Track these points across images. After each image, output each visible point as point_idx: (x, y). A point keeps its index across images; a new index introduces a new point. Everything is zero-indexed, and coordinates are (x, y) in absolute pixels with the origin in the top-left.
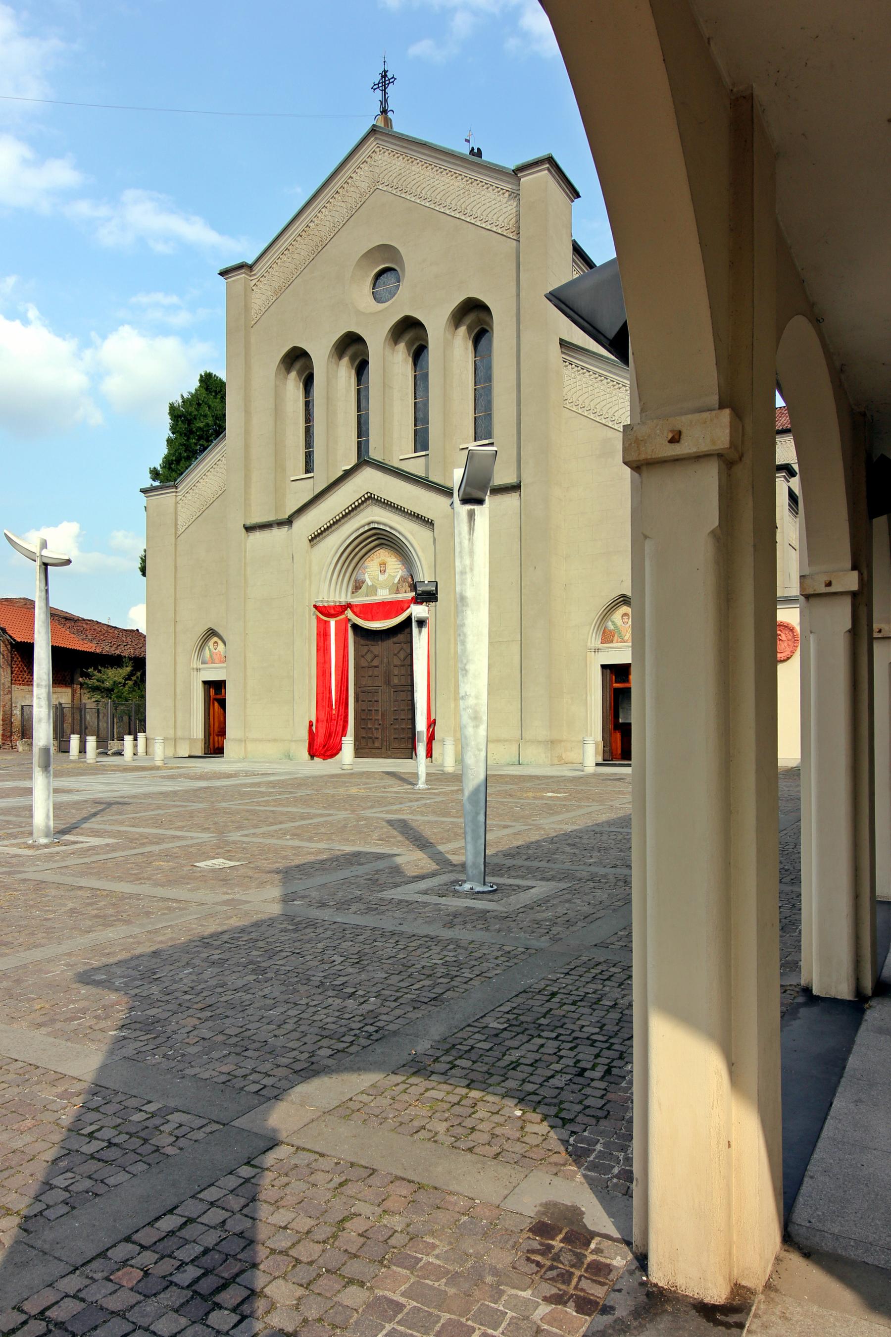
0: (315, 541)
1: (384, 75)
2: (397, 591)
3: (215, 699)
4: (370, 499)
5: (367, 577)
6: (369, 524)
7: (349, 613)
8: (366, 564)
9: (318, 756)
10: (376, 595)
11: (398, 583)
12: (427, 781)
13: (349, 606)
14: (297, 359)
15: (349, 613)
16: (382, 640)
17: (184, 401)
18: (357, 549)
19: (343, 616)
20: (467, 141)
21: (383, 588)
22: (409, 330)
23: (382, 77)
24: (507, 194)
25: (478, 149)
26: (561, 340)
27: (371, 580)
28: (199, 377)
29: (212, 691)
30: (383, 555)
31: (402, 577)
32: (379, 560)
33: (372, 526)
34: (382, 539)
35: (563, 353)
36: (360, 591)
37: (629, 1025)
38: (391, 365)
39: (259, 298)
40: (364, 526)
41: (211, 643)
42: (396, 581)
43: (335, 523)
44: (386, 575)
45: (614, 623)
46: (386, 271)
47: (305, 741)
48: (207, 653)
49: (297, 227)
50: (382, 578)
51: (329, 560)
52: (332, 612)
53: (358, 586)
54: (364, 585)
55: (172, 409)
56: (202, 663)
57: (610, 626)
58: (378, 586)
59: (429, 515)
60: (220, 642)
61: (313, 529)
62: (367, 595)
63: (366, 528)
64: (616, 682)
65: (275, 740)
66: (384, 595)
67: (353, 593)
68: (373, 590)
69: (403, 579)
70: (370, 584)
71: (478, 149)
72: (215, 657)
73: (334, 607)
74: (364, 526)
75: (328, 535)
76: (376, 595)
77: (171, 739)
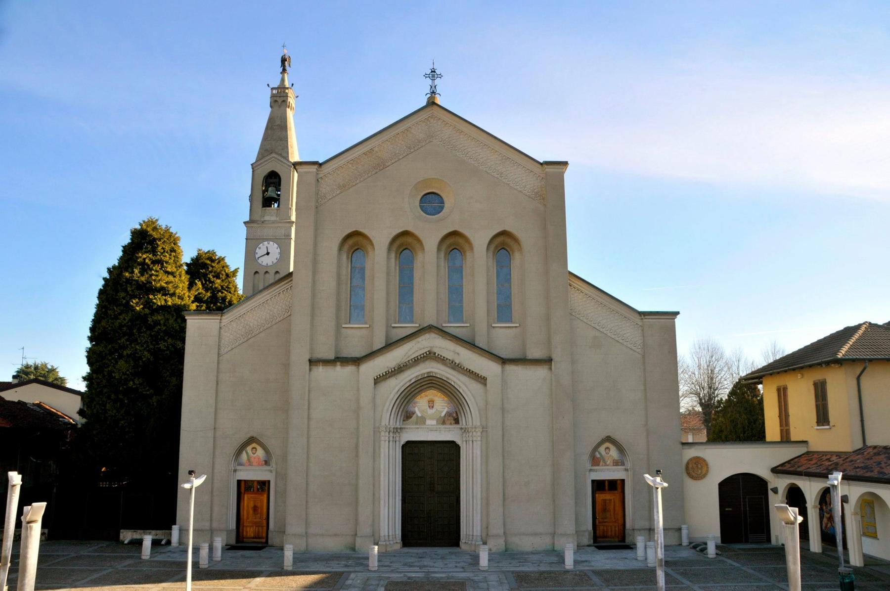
5: (416, 410)
8: (416, 400)
14: (355, 242)
17: (192, 259)
22: (454, 243)
27: (420, 412)
30: (432, 394)
31: (447, 412)
34: (430, 382)
37: (279, 552)
41: (249, 449)
42: (443, 414)
44: (434, 410)
45: (600, 453)
46: (431, 202)
48: (244, 456)
50: (430, 412)
51: (392, 396)
54: (414, 416)
55: (109, 269)
59: (482, 373)
60: (258, 448)
61: (381, 371)
65: (336, 535)
69: (449, 414)
70: (419, 415)
72: (252, 460)
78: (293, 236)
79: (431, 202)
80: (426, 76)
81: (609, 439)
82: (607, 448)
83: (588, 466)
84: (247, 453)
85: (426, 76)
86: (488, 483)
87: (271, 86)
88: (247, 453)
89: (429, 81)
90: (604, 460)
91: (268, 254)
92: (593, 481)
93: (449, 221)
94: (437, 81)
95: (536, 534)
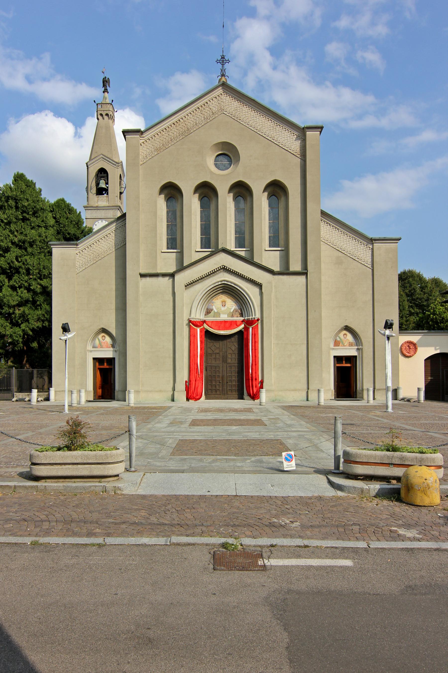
0: (188, 287)
1: (223, 57)
2: (232, 316)
3: (99, 369)
4: (225, 269)
5: (214, 307)
6: (221, 281)
7: (205, 326)
8: (214, 301)
9: (191, 399)
10: (220, 317)
11: (233, 312)
12: (393, 408)
13: (204, 322)
15: (205, 326)
16: (222, 341)
18: (211, 293)
19: (202, 327)
20: (103, 73)
21: (224, 313)
23: (222, 58)
24: (295, 136)
25: (108, 78)
26: (321, 210)
28: (13, 175)
29: (97, 364)
31: (235, 309)
32: (221, 300)
33: (224, 282)
35: (321, 216)
36: (210, 314)
38: (227, 204)
39: (144, 151)
40: (218, 282)
41: (100, 337)
42: (232, 311)
43: (202, 279)
44: (226, 307)
45: (339, 338)
46: (228, 154)
47: (183, 391)
48: (97, 342)
49: (173, 119)
50: (223, 309)
52: (198, 324)
53: (208, 312)
54: (212, 312)
56: (93, 347)
57: (338, 339)
58: (220, 313)
62: (214, 317)
63: (220, 283)
64: (337, 363)
65: (160, 391)
66: (224, 317)
67: (205, 315)
68: (218, 314)
70: (216, 311)
71: (108, 78)
72: (103, 344)
73: (199, 322)
74: (218, 282)
75: (196, 284)
76: (220, 317)
77: (384, 389)
78: (67, 380)
79: (228, 154)
80: (217, 61)
81: (347, 328)
82: (345, 334)
83: (332, 346)
84: (99, 340)
85: (217, 61)
86: (190, 341)
87: (97, 102)
88: (99, 340)
89: (220, 66)
90: (343, 342)
91: (72, 392)
92: (335, 357)
93: (235, 174)
94: (226, 66)
95: (295, 390)
